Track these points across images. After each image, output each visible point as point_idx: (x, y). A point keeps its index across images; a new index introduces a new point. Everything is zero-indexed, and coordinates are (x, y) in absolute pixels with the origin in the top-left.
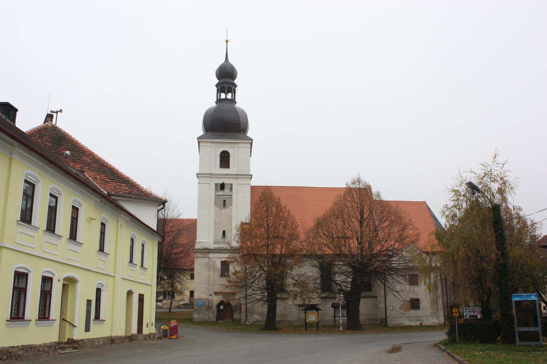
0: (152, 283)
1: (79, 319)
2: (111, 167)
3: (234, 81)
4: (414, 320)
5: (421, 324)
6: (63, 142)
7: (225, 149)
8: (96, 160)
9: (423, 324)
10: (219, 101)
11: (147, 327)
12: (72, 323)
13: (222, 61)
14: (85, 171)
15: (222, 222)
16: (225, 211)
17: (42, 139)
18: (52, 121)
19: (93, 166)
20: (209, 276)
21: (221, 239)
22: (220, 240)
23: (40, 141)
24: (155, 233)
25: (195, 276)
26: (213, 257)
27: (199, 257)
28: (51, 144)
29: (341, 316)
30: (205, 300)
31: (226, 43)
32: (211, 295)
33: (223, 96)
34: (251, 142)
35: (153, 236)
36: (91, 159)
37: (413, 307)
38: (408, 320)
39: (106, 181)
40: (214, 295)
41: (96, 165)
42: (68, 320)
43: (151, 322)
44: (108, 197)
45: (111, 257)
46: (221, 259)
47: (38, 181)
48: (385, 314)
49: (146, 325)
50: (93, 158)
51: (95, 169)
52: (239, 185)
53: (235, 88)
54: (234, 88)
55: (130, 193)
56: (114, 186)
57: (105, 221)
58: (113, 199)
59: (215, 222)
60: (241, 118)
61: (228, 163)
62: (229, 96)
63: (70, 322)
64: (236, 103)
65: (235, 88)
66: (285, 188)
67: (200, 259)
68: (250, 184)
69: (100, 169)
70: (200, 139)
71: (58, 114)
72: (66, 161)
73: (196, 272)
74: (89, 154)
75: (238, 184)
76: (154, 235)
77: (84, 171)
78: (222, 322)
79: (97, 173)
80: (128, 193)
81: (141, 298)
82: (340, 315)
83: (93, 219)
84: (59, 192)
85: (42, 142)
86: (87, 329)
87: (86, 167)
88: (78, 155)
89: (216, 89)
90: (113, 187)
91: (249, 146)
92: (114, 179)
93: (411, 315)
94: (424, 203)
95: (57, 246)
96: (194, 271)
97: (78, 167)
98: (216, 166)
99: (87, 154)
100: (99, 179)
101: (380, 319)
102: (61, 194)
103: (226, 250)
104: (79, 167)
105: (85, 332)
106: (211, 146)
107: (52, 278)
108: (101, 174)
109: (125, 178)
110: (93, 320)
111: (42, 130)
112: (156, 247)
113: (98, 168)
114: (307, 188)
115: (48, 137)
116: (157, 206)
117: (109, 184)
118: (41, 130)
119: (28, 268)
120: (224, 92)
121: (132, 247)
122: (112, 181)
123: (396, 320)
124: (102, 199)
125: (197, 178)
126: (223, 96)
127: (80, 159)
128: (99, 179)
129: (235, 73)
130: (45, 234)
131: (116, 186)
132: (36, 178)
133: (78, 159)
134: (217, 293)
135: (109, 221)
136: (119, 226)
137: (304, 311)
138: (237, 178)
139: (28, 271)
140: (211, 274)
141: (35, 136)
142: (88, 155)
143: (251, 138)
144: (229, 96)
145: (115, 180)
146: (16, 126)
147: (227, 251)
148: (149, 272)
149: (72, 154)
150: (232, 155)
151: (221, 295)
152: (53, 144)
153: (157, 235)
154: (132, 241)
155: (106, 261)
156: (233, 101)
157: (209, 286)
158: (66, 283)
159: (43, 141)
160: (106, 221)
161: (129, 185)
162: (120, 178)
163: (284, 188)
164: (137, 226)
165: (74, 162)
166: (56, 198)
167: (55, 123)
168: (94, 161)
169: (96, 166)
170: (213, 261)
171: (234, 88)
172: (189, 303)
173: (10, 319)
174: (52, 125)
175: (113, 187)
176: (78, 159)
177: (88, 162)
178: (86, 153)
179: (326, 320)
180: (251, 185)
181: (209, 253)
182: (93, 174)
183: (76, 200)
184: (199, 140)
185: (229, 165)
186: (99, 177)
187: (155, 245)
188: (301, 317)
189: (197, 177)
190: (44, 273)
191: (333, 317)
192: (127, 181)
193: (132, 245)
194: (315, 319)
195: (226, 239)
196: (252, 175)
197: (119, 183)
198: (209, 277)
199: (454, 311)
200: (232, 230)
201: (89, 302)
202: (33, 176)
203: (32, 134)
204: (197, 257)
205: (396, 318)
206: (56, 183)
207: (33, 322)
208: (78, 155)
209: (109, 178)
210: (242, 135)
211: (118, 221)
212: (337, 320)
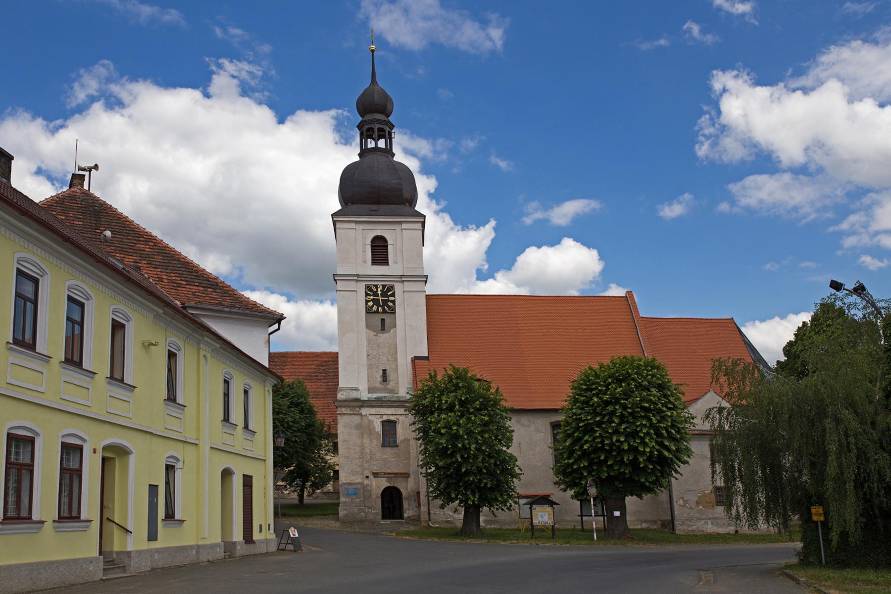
0: (265, 456)
1: (137, 520)
2: (186, 261)
3: (389, 118)
4: (724, 524)
5: (737, 532)
6: (103, 220)
7: (379, 233)
9: (740, 532)
11: (261, 531)
12: (124, 527)
14: (142, 268)
15: (380, 355)
16: (383, 337)
17: (67, 215)
18: (82, 185)
19: (156, 260)
20: (362, 445)
21: (381, 384)
22: (378, 385)
23: (63, 218)
24: (266, 372)
25: (340, 445)
26: (368, 414)
27: (344, 414)
28: (81, 223)
29: (593, 515)
30: (359, 486)
32: (367, 477)
33: (371, 144)
34: (423, 220)
36: (152, 247)
37: (720, 502)
38: (712, 524)
39: (179, 284)
40: (372, 477)
41: (160, 257)
42: (116, 521)
43: (268, 523)
44: (184, 311)
45: (190, 411)
46: (382, 418)
47: (44, 273)
48: (669, 513)
50: (155, 246)
51: (159, 264)
56: (193, 292)
57: (175, 349)
58: (191, 314)
59: (368, 355)
61: (386, 256)
62: (382, 144)
63: (119, 523)
67: (346, 417)
68: (425, 291)
69: (167, 265)
70: (335, 217)
71: (92, 172)
72: (109, 250)
73: (340, 440)
75: (404, 292)
77: (141, 267)
78: (389, 522)
79: (164, 271)
80: (216, 304)
81: (248, 481)
82: (592, 513)
83: (152, 344)
84: (178, 346)
85: (67, 219)
86: (152, 536)
87: (144, 260)
88: (129, 241)
90: (191, 293)
91: (419, 226)
92: (191, 280)
93: (716, 515)
95: (88, 390)
96: (337, 438)
97: (129, 260)
98: (366, 262)
101: (661, 521)
102: (130, 319)
103: (389, 402)
104: (132, 260)
105: (149, 540)
106: (355, 229)
107: (82, 446)
108: (170, 273)
109: (211, 278)
110: (162, 520)
111: (65, 199)
112: (269, 394)
113: (164, 263)
115: (76, 212)
116: (268, 326)
117: (185, 289)
118: (65, 200)
119: (32, 428)
120: (372, 138)
121: (227, 395)
122: (189, 283)
123: (691, 523)
124: (166, 308)
125: (335, 282)
126: (371, 144)
127: (133, 248)
128: (166, 281)
130: (63, 368)
131: (196, 292)
132: (39, 267)
133: (130, 247)
134: (378, 473)
135: (183, 349)
136: (202, 360)
137: (529, 506)
138: (403, 282)
139: (34, 434)
140: (366, 441)
141: (55, 210)
142: (146, 241)
143: (423, 214)
144: (382, 144)
146: (13, 186)
147: (391, 403)
148: (259, 437)
149: (113, 236)
151: (385, 477)
152: (85, 224)
153: (269, 374)
154: (226, 385)
155: (180, 419)
157: (363, 462)
158: (109, 455)
159: (68, 218)
160: (126, 320)
162: (201, 278)
163: (482, 297)
164: (235, 358)
165: (122, 253)
166: (82, 305)
167: (87, 189)
169: (161, 259)
170: (368, 421)
172: (332, 490)
173: (3, 520)
174: (82, 191)
175: (191, 293)
176: (130, 247)
177: (147, 253)
178: (143, 237)
179: (566, 521)
180: (427, 294)
181: (361, 407)
182: (155, 273)
183: (174, 343)
184: (334, 219)
185: (388, 260)
186: (166, 277)
187: (266, 391)
188: (523, 516)
189: (335, 280)
190: (63, 438)
191: (579, 516)
192: (215, 284)
193: (226, 392)
194: (549, 519)
195: (388, 384)
197: (201, 287)
198: (362, 446)
199: (813, 511)
200: (397, 369)
201: (153, 489)
202: (32, 262)
203: (49, 206)
204: (340, 414)
205: (690, 520)
206: (99, 289)
207: (48, 527)
208: (129, 241)
209: (183, 279)
210: (407, 208)
211: (199, 349)
212: (585, 521)
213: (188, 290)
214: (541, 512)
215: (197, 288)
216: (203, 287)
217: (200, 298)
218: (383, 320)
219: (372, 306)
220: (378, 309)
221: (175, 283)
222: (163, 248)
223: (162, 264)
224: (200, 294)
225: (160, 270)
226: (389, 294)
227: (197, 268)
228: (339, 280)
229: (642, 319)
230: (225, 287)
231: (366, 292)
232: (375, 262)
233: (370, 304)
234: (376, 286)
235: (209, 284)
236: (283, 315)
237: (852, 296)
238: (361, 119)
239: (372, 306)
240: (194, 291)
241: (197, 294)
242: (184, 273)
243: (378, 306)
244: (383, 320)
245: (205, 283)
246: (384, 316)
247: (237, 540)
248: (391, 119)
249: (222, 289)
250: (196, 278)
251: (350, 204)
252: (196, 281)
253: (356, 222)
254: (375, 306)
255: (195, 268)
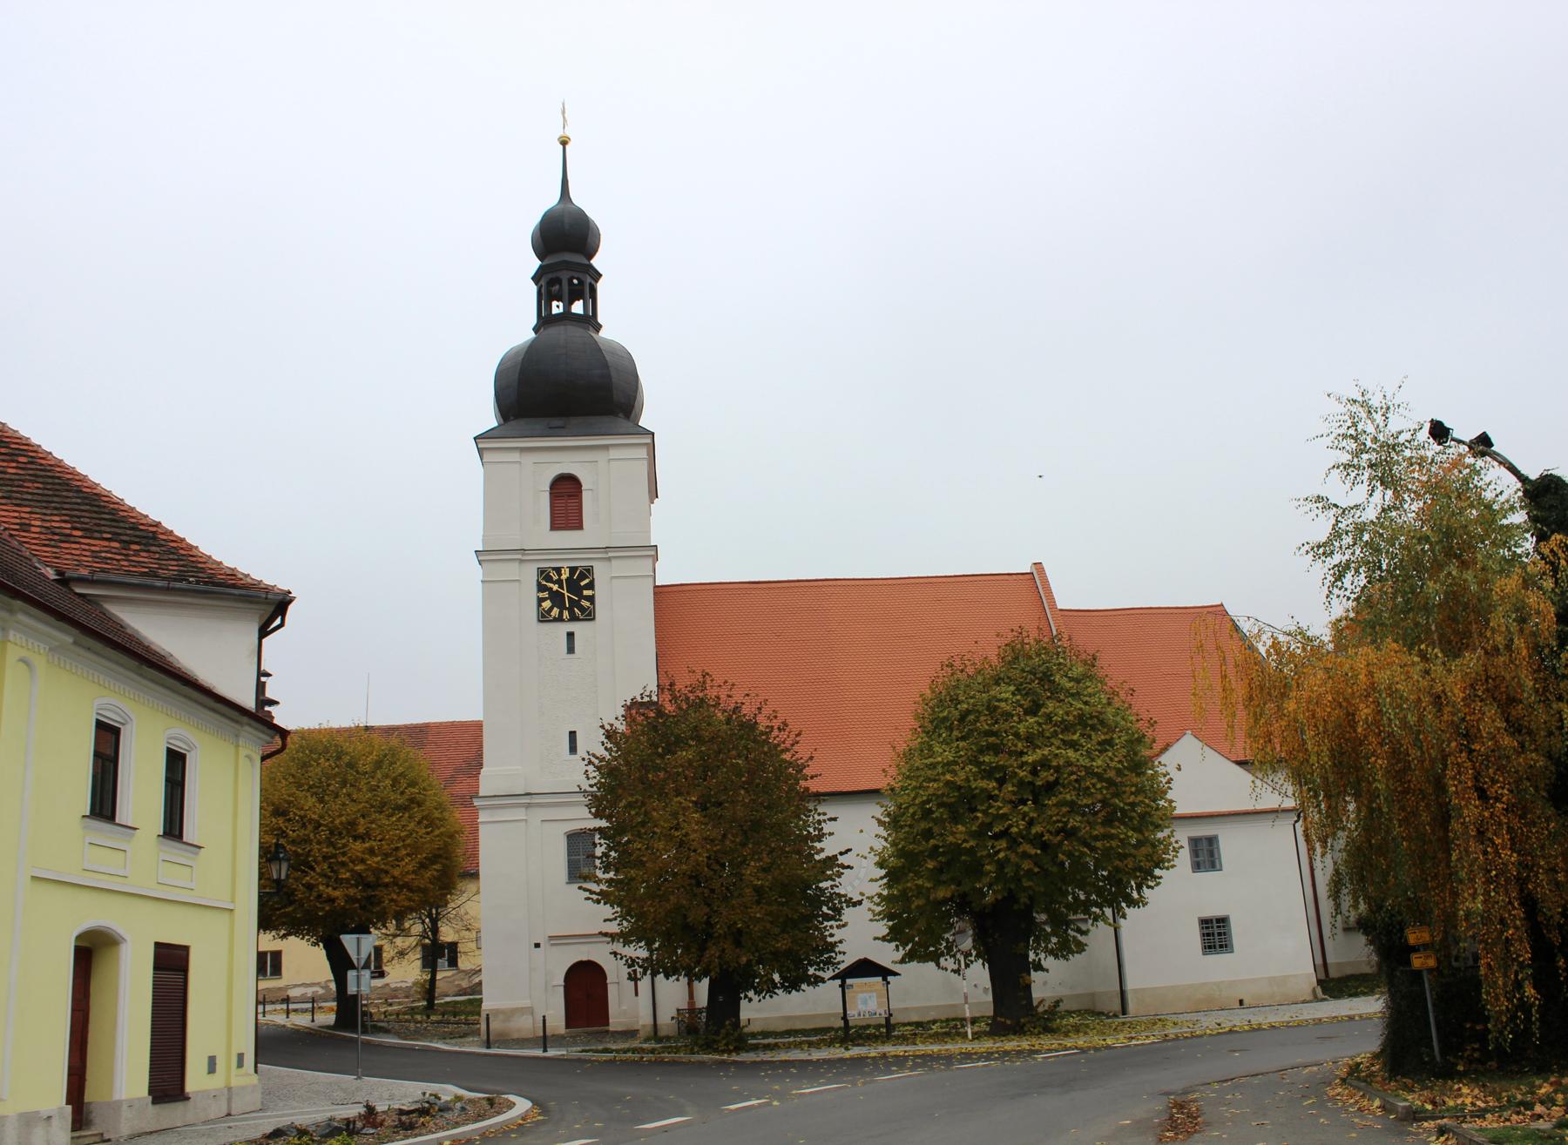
3: (592, 262)
8: (41, 470)
10: (545, 321)
13: (552, 199)
31: (561, 146)
35: (233, 724)
37: (1210, 947)
49: (218, 1067)
52: (614, 581)
53: (593, 282)
54: (589, 280)
55: (152, 574)
60: (613, 374)
64: (598, 327)
65: (593, 282)
66: (769, 585)
74: (17, 452)
76: (237, 722)
89: (534, 289)
90: (88, 554)
91: (643, 453)
94: (1219, 611)
99: (11, 451)
100: (38, 530)
114: (839, 583)
126: (557, 308)
128: (38, 530)
129: (589, 240)
137: (839, 982)
138: (609, 559)
145: (101, 532)
150: (591, 487)
156: (590, 321)
161: (153, 549)
162: (122, 525)
168: (31, 472)
169: (38, 488)
171: (589, 280)
182: (16, 514)
184: (479, 446)
194: (879, 1004)
196: (656, 546)
197: (116, 541)
210: (622, 423)
213: (83, 547)
214: (862, 992)
215: (106, 543)
216: (121, 542)
217: (107, 564)
218: (571, 635)
219: (551, 609)
220: (561, 614)
221: (57, 534)
222: (49, 468)
223: (40, 498)
224: (109, 555)
225: (28, 509)
226: (582, 584)
227: (116, 506)
228: (484, 560)
229: (1063, 613)
230: (173, 541)
231: (539, 584)
232: (557, 524)
233: (547, 604)
234: (558, 570)
235: (135, 536)
236: (290, 593)
237: (1381, 1035)
238: (540, 262)
239: (551, 609)
240: (97, 549)
241: (103, 555)
242: (83, 514)
243: (562, 607)
244: (571, 635)
245: (126, 535)
246: (573, 626)
247: (123, 1097)
248: (595, 262)
249: (163, 546)
250: (109, 523)
251: (512, 418)
252: (108, 529)
253: (523, 450)
254: (555, 609)
255: (112, 506)
